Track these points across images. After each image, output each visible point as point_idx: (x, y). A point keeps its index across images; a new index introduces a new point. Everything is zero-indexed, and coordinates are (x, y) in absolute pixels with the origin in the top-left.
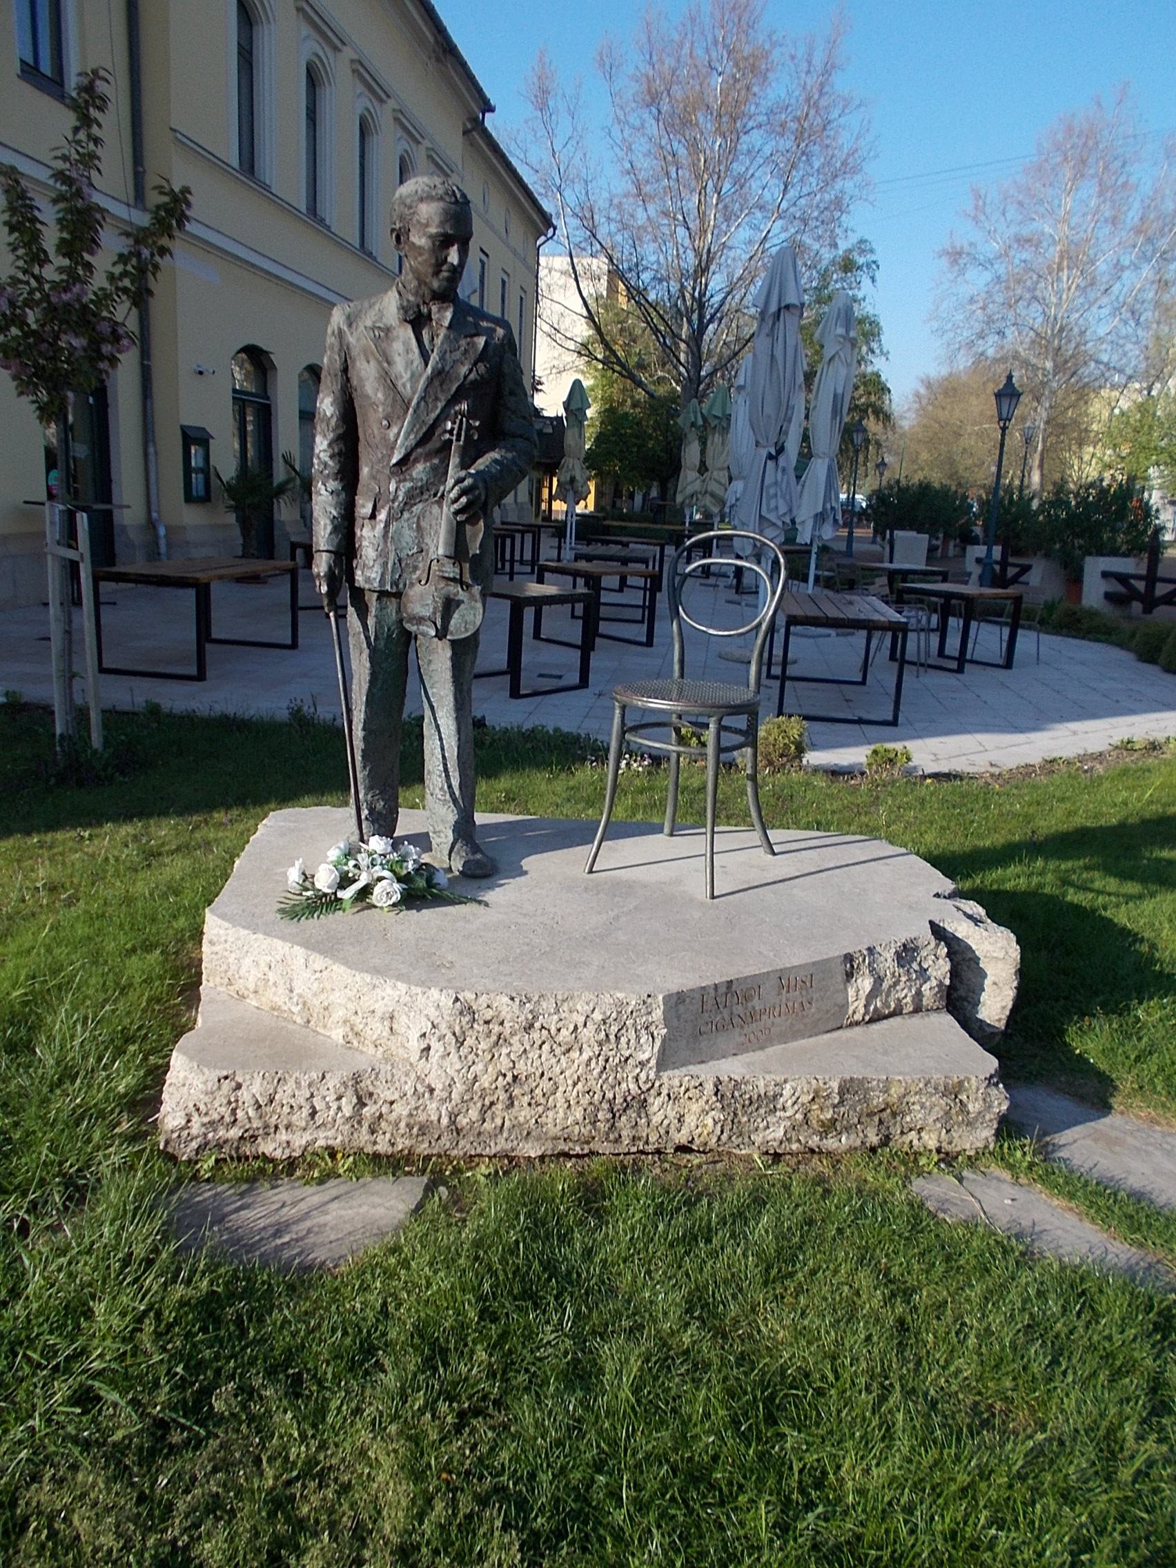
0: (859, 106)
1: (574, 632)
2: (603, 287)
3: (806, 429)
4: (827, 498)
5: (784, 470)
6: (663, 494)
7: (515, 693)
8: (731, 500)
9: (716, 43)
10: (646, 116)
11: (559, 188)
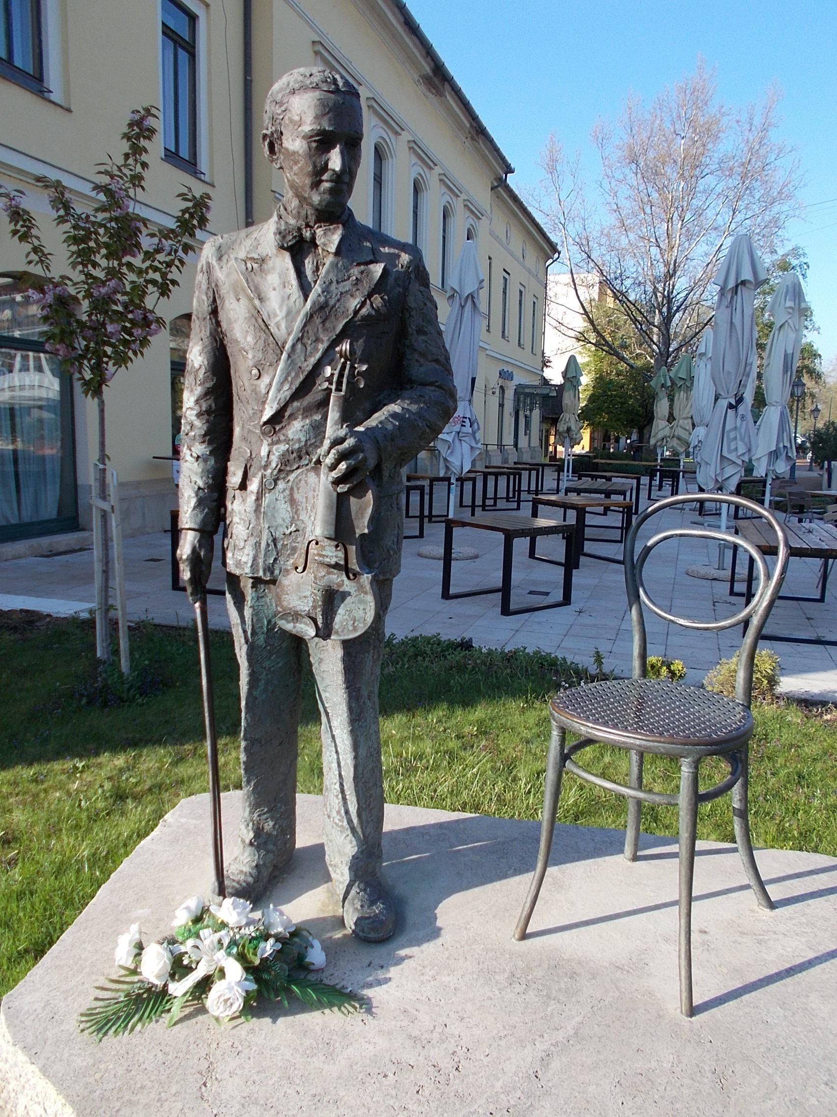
0: (791, 151)
1: (560, 554)
2: (595, 293)
3: (759, 387)
4: (780, 438)
5: (743, 417)
6: (641, 439)
7: (506, 611)
8: (694, 442)
9: (679, 117)
10: (627, 171)
11: (563, 225)
